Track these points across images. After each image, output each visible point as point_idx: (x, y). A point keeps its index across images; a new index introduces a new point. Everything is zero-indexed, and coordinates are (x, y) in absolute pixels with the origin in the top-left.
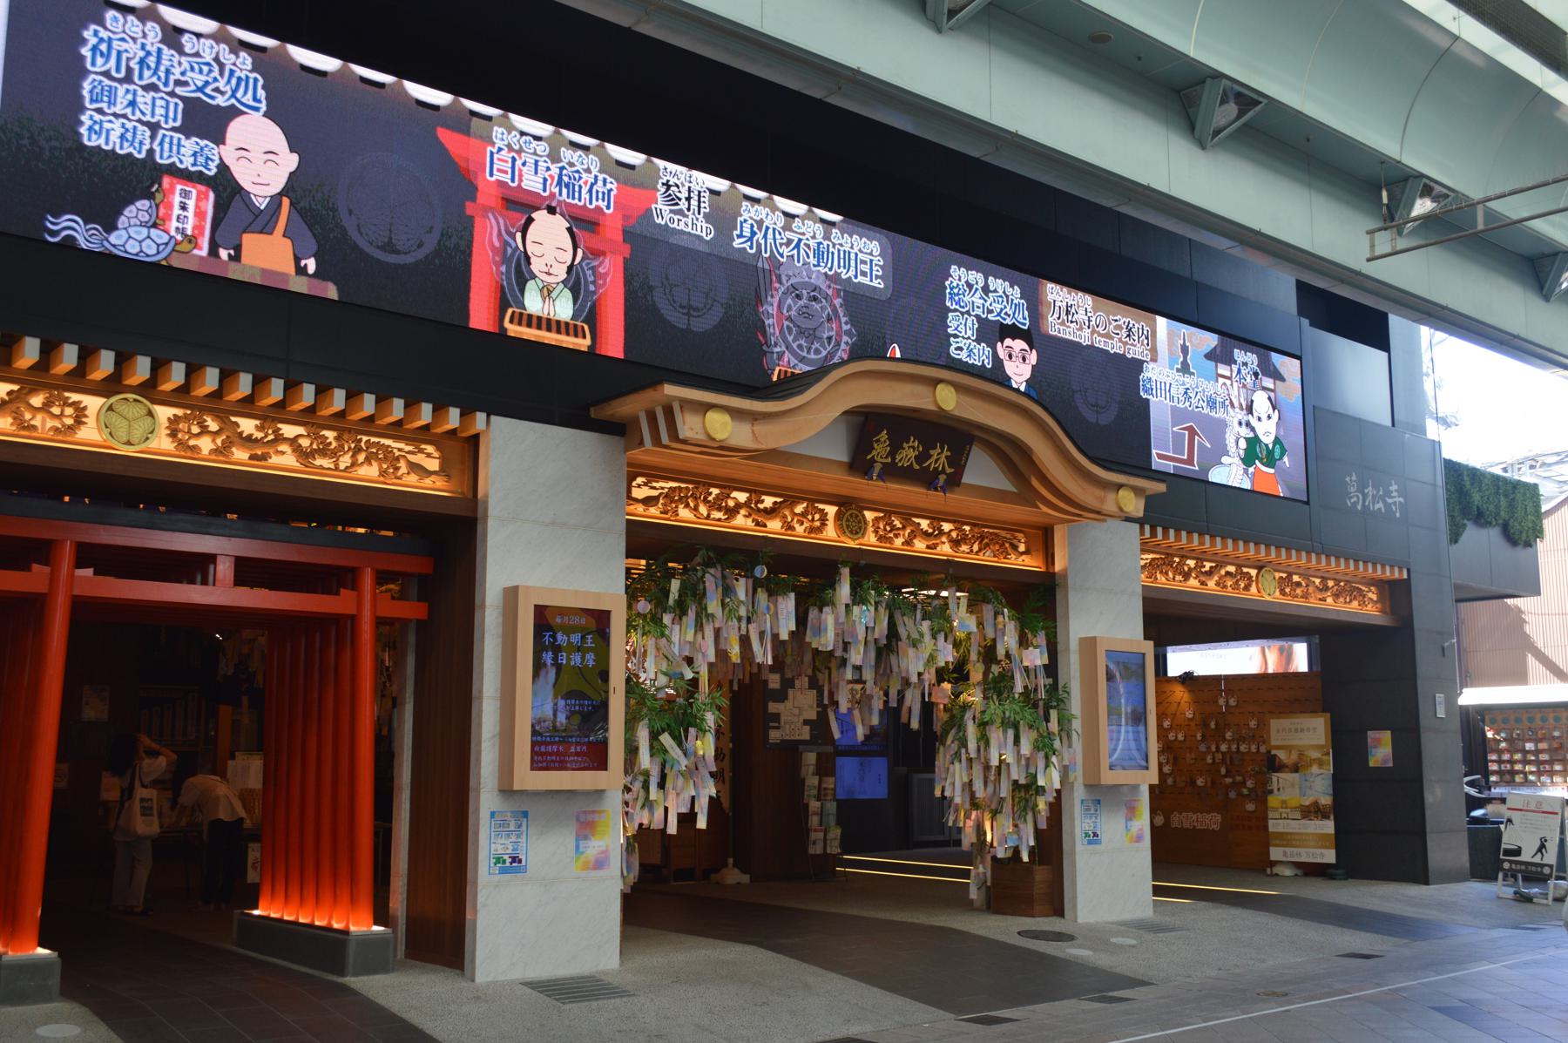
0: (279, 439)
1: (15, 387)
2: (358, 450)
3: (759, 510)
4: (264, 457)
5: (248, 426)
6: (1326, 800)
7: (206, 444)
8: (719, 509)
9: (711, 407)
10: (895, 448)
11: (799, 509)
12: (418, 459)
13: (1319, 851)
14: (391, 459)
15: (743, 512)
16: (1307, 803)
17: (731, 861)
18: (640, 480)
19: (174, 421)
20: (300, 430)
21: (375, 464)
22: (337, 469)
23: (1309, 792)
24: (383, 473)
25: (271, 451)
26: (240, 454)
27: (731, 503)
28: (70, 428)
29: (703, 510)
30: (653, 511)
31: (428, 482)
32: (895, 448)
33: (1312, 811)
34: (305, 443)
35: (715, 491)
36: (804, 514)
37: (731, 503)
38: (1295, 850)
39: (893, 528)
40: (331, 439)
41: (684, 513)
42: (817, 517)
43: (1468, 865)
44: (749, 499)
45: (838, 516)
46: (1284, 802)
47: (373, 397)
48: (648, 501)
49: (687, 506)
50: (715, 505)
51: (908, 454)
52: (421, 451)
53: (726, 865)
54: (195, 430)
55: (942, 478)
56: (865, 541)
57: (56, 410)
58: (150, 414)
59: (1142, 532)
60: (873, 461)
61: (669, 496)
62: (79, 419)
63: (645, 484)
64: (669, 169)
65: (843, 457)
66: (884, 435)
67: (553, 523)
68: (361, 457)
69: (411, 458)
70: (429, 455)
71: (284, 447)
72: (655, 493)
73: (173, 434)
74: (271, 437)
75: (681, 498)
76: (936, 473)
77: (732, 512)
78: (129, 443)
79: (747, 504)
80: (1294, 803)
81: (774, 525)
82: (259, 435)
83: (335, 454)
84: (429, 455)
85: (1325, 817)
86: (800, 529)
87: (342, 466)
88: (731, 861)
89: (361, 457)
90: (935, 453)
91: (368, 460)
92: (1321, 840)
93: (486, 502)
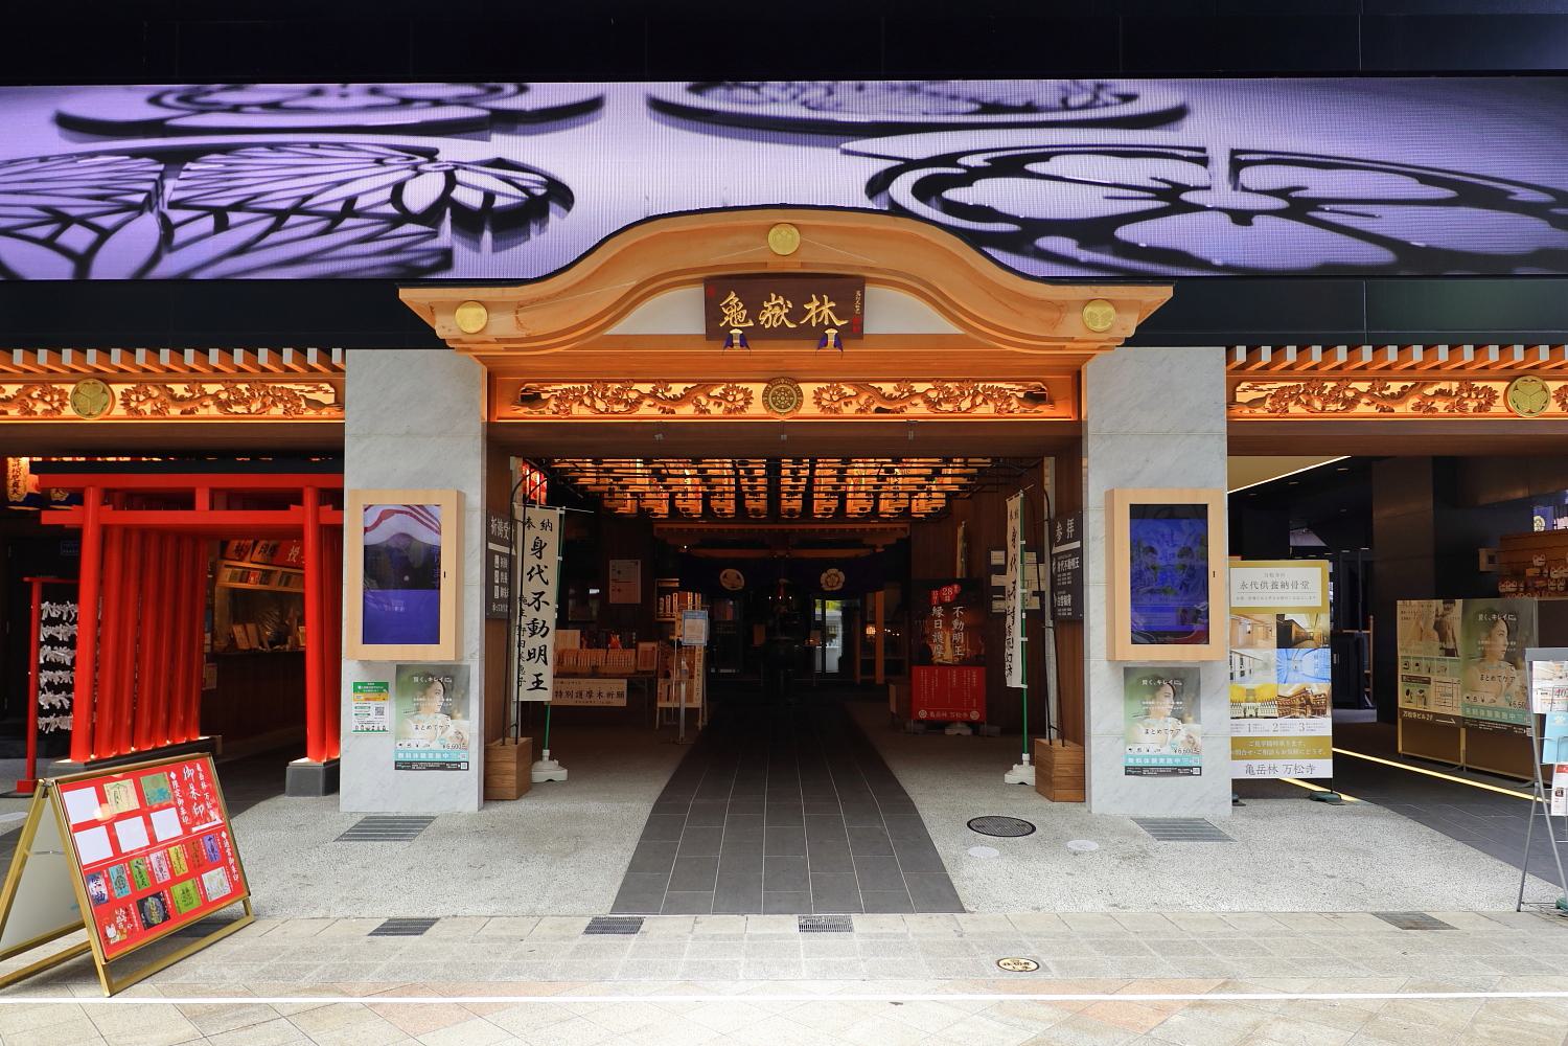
0: (913, 394)
1: (21, 386)
2: (976, 394)
3: (1384, 396)
4: (192, 412)
5: (179, 389)
6: (1322, 688)
7: (147, 408)
8: (1336, 400)
9: (462, 303)
10: (754, 309)
11: (717, 391)
12: (319, 396)
13: (1305, 763)
14: (294, 397)
15: (1365, 400)
16: (1290, 693)
17: (546, 752)
18: (1244, 385)
19: (126, 395)
20: (219, 387)
21: (281, 406)
22: (250, 412)
23: (1292, 676)
24: (999, 410)
25: (907, 404)
26: (175, 411)
27: (1350, 394)
28: (742, 408)
29: (600, 405)
30: (1259, 411)
31: (325, 413)
32: (754, 309)
33: (1305, 704)
34: (933, 395)
35: (1330, 385)
36: (724, 397)
37: (633, 396)
38: (1267, 763)
39: (843, 397)
40: (244, 391)
41: (1295, 409)
42: (740, 396)
43: (903, 785)
44: (1373, 388)
45: (765, 394)
46: (1250, 692)
47: (1345, 347)
48: (1253, 403)
49: (1298, 402)
50: (1333, 397)
51: (774, 312)
52: (320, 389)
53: (541, 758)
54: (142, 398)
55: (831, 332)
56: (803, 412)
57: (48, 398)
58: (1545, 389)
59: (1230, 358)
60: (728, 327)
61: (1278, 396)
62: (748, 401)
63: (1251, 388)
64: (866, 82)
65: (703, 331)
66: (733, 298)
67: (408, 433)
68: (979, 400)
69: (309, 396)
70: (327, 392)
71: (918, 400)
72: (1261, 395)
73: (126, 404)
74: (906, 394)
75: (1291, 397)
76: (821, 327)
77: (1350, 403)
78: (1530, 412)
79: (653, 395)
80: (1268, 694)
81: (1405, 409)
82: (188, 395)
83: (246, 402)
84: (327, 392)
85: (1318, 711)
86: (40, 407)
87: (253, 409)
88: (546, 752)
89: (979, 400)
90: (812, 307)
91: (274, 404)
92: (1310, 746)
93: (1086, 423)
